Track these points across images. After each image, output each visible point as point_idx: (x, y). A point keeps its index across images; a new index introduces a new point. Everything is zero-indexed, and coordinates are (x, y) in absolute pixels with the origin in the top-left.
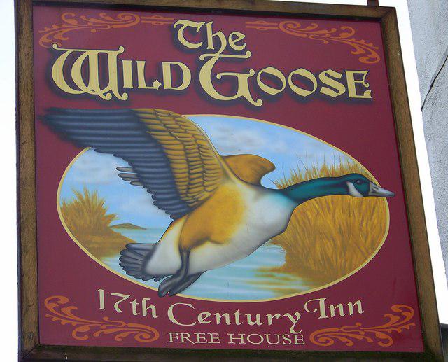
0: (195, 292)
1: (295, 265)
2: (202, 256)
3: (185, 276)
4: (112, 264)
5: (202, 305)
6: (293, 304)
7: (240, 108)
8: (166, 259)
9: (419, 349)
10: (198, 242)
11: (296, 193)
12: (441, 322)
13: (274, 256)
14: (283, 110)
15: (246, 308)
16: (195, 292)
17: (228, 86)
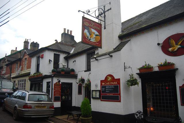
0: (91, 40)
1: (96, 40)
2: (91, 38)
3: (90, 39)
4: (87, 37)
5: (91, 41)
6: (95, 42)
7: (93, 29)
8: (89, 38)
9: (54, 111)
10: (91, 37)
11: (96, 35)
12: (60, 106)
13: (94, 39)
14: (95, 29)
15: (94, 42)
16: (91, 40)
17: (93, 27)
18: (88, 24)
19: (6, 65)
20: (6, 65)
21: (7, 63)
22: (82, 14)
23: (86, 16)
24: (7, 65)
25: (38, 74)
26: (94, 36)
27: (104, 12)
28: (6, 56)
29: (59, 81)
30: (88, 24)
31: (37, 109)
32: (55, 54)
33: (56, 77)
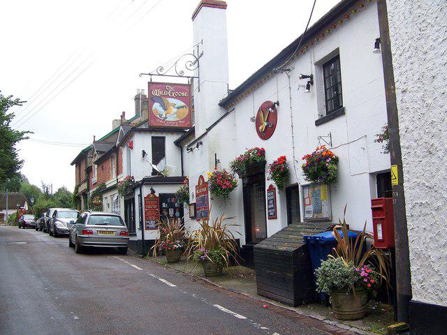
1: (178, 117)
3: (166, 118)
8: (164, 116)
18: (161, 93)
19: (95, 163)
20: (95, 163)
21: (98, 157)
22: (148, 79)
23: (156, 79)
24: (98, 163)
25: (334, 166)
26: (175, 110)
27: (197, 60)
28: (94, 142)
29: (153, 192)
30: (161, 93)
31: (100, 235)
32: (152, 137)
33: (146, 184)
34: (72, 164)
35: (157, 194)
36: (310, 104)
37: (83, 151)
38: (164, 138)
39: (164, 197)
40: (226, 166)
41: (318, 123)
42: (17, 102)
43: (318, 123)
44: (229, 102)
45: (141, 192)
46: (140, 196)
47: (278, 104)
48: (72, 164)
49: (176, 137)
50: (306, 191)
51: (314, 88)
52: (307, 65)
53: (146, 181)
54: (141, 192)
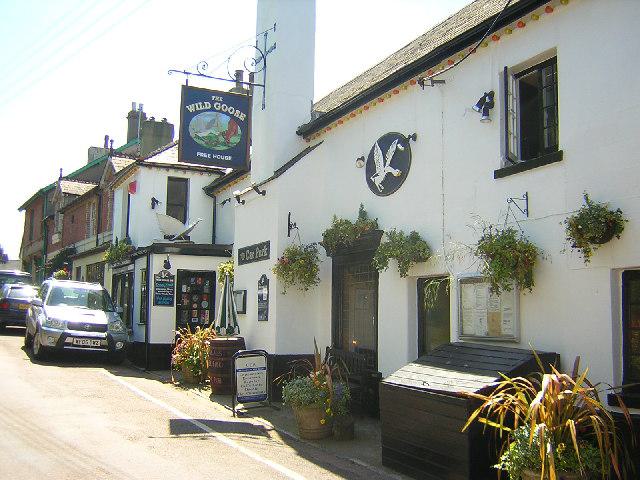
22: (181, 80)
23: (197, 83)
29: (167, 265)
32: (170, 178)
34: (20, 209)
35: (173, 271)
36: (489, 141)
37: (41, 191)
38: (171, 304)
39: (184, 275)
40: (313, 231)
41: (499, 174)
42: (335, 217)
43: (499, 174)
44: (317, 126)
45: (148, 265)
46: (147, 272)
47: (414, 137)
48: (20, 209)
49: (207, 180)
50: (470, 291)
51: (497, 111)
52: (483, 71)
53: (157, 248)
54: (148, 265)
